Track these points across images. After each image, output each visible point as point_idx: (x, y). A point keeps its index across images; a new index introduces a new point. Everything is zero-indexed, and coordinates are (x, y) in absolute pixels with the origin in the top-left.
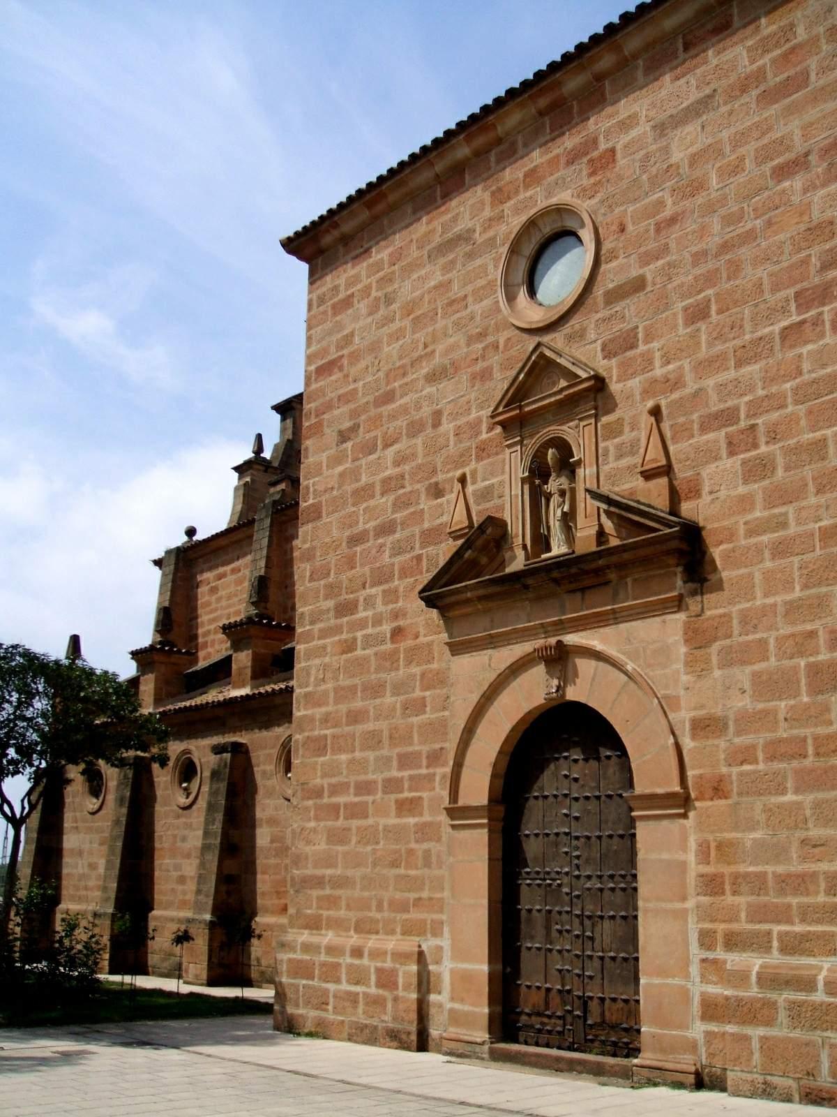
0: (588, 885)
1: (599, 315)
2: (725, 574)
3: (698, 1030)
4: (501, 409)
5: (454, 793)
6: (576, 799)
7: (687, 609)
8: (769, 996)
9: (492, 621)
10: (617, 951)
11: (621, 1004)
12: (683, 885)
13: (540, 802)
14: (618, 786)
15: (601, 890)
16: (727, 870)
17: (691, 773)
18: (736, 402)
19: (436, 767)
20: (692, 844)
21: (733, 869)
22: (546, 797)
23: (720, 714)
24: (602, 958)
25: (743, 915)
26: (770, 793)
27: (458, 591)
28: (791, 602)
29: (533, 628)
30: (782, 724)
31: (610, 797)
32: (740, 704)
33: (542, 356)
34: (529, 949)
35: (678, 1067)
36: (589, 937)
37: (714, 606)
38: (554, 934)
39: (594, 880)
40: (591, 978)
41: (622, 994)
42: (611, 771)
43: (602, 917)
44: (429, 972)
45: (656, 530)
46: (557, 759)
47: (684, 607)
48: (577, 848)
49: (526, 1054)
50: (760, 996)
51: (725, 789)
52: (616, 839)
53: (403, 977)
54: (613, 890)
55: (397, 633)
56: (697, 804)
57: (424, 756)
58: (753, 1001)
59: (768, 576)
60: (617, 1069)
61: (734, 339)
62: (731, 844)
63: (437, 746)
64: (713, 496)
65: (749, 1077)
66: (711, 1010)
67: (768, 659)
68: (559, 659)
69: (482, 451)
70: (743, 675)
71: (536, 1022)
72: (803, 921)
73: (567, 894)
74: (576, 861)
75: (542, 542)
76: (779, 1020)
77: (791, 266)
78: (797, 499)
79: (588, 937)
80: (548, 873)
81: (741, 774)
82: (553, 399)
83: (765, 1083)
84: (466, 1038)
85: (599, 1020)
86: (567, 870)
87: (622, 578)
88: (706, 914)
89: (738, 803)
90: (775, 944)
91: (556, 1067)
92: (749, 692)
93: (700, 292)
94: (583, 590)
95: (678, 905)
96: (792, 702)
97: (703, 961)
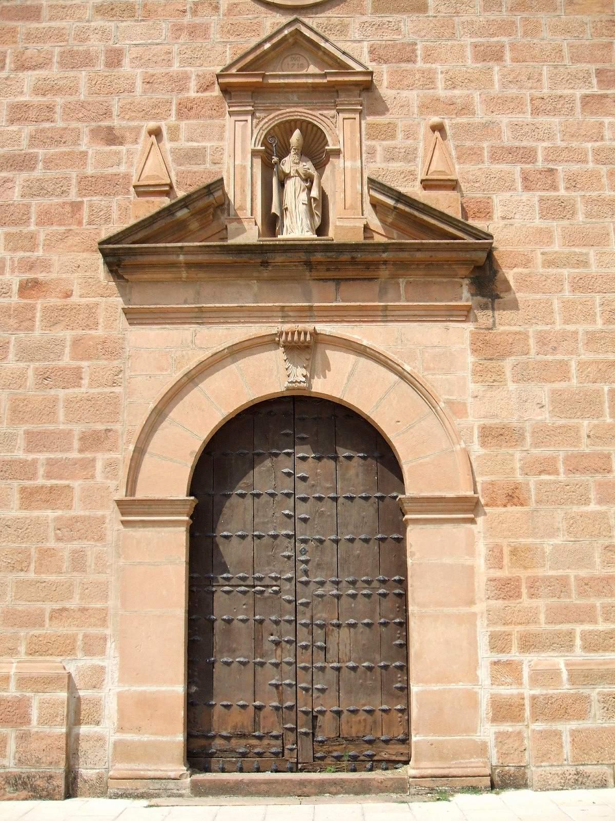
0: (320, 591)
1: (364, 18)
2: (519, 296)
3: (487, 732)
4: (234, 71)
5: (132, 483)
6: (304, 500)
7: (476, 320)
8: (581, 691)
9: (198, 293)
10: (360, 660)
11: (362, 716)
12: (472, 590)
13: (249, 501)
14: (362, 488)
15: (338, 597)
16: (523, 574)
17: (479, 479)
18: (534, 144)
19: (97, 451)
20: (482, 548)
21: (530, 572)
22: (258, 495)
23: (515, 425)
24: (338, 669)
25: (542, 617)
26: (572, 503)
27: (156, 252)
28: (593, 333)
29: (270, 309)
30: (585, 440)
31: (351, 499)
32: (539, 418)
33: (298, 31)
34: (228, 664)
35: (469, 771)
36: (320, 648)
37: (506, 322)
38: (268, 646)
39: (328, 586)
40: (322, 691)
41: (364, 705)
42: (352, 472)
43: (339, 626)
44: (79, 699)
45: (456, 237)
46: (276, 455)
47: (472, 318)
48: (304, 552)
49: (252, 783)
50: (572, 691)
51: (521, 497)
52: (358, 544)
53: (40, 708)
54: (354, 596)
55: (29, 288)
56: (487, 509)
57: (76, 437)
58: (563, 697)
59: (567, 306)
60: (389, 783)
61: (531, 88)
62: (528, 549)
63: (100, 427)
64: (506, 222)
65: (559, 770)
66: (504, 711)
67: (569, 379)
68: (303, 349)
69: (186, 110)
70: (543, 392)
71: (240, 746)
72: (606, 620)
73: (289, 602)
74: (303, 566)
75: (272, 223)
76: (593, 712)
77: (593, 45)
78: (599, 244)
79: (319, 647)
80: (260, 579)
81: (541, 484)
82: (310, 81)
83: (578, 773)
84: (151, 774)
85: (333, 735)
86: (289, 575)
87: (394, 277)
88: (494, 618)
89: (536, 510)
90: (578, 642)
91: (299, 792)
92: (548, 407)
93: (493, 35)
94: (338, 281)
95: (464, 610)
96: (595, 422)
97: (495, 663)
